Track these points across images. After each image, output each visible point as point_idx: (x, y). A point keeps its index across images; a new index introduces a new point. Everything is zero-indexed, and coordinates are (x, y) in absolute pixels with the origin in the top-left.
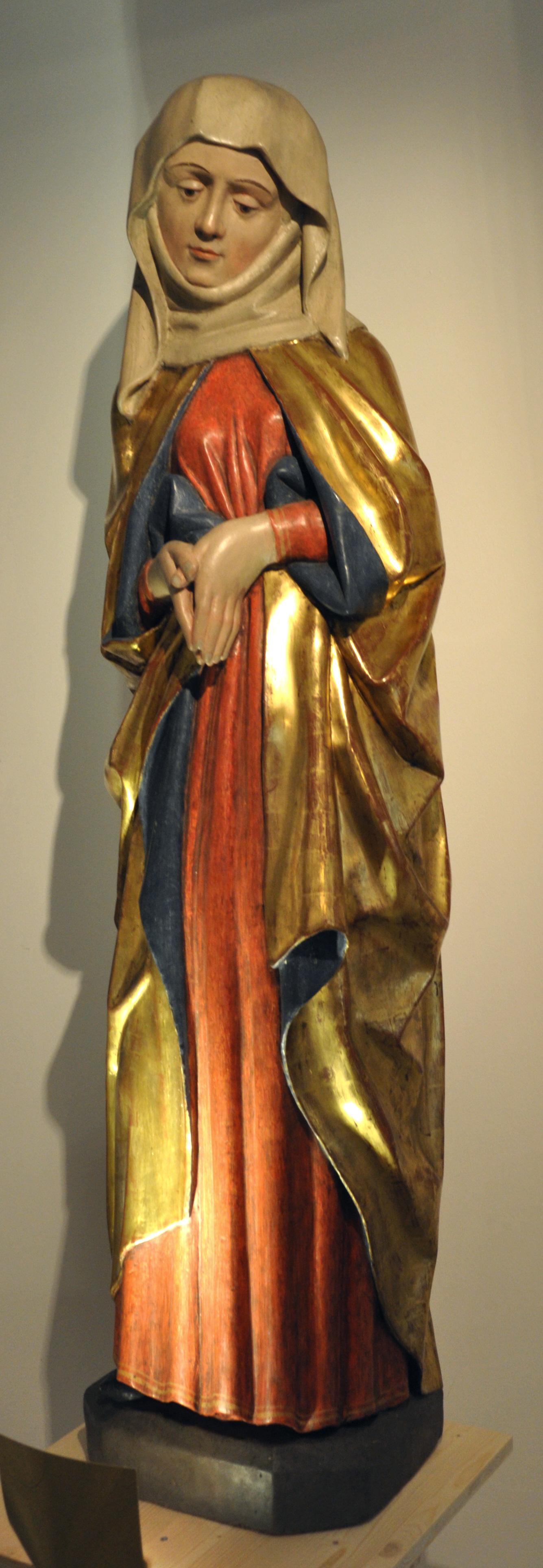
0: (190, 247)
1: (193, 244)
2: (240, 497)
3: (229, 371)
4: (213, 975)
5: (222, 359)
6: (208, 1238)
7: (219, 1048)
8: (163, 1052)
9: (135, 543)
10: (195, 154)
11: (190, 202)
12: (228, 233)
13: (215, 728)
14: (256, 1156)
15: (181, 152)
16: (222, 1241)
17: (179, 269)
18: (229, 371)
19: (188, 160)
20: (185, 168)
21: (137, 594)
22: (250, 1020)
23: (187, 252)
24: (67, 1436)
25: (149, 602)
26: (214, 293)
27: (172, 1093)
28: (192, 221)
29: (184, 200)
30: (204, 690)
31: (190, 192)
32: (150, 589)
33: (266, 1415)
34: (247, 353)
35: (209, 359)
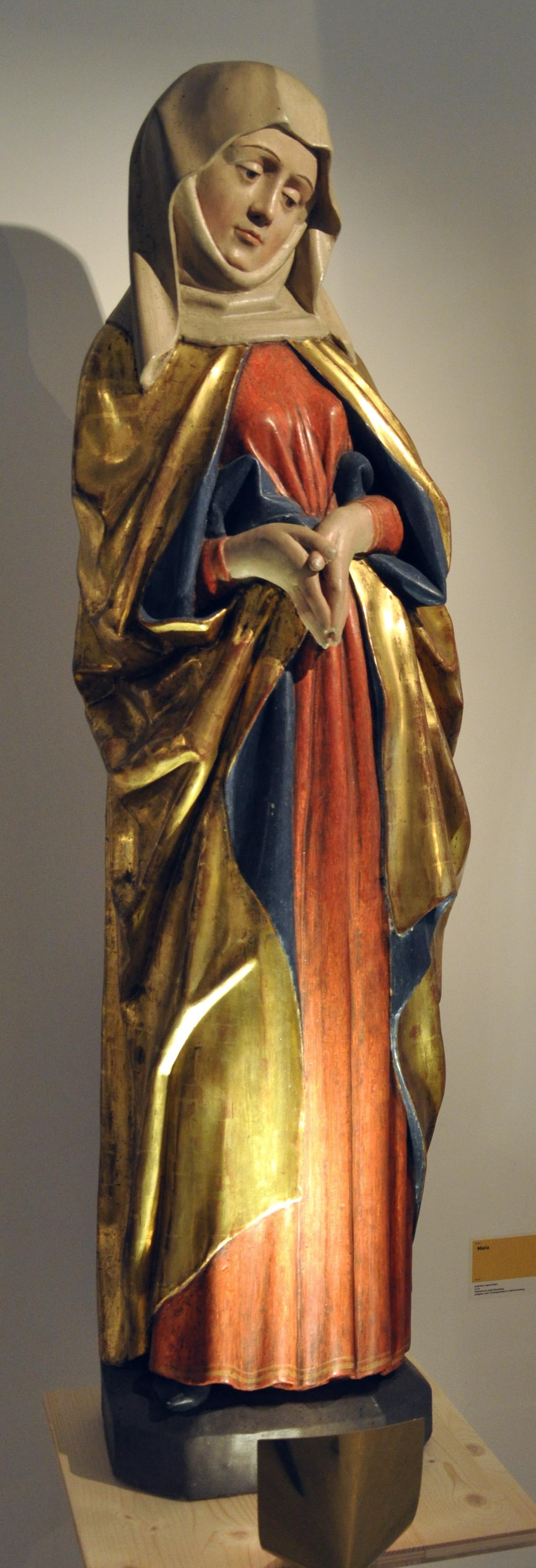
0: (237, 228)
1: (241, 226)
2: (312, 486)
3: (273, 358)
4: (337, 951)
5: (263, 345)
6: (314, 1211)
7: (341, 1021)
8: (268, 1036)
9: (201, 519)
10: (273, 142)
11: (249, 184)
12: (274, 222)
13: (324, 710)
14: (367, 1119)
15: (257, 133)
16: (342, 1208)
17: (218, 247)
18: (273, 358)
19: (265, 144)
20: (259, 150)
21: (200, 575)
22: (360, 990)
23: (232, 232)
24: (69, 1486)
25: (219, 582)
26: (254, 275)
27: (276, 1076)
28: (247, 205)
29: (242, 180)
30: (305, 673)
31: (252, 174)
32: (228, 570)
33: (371, 1367)
34: (285, 343)
35: (247, 343)
